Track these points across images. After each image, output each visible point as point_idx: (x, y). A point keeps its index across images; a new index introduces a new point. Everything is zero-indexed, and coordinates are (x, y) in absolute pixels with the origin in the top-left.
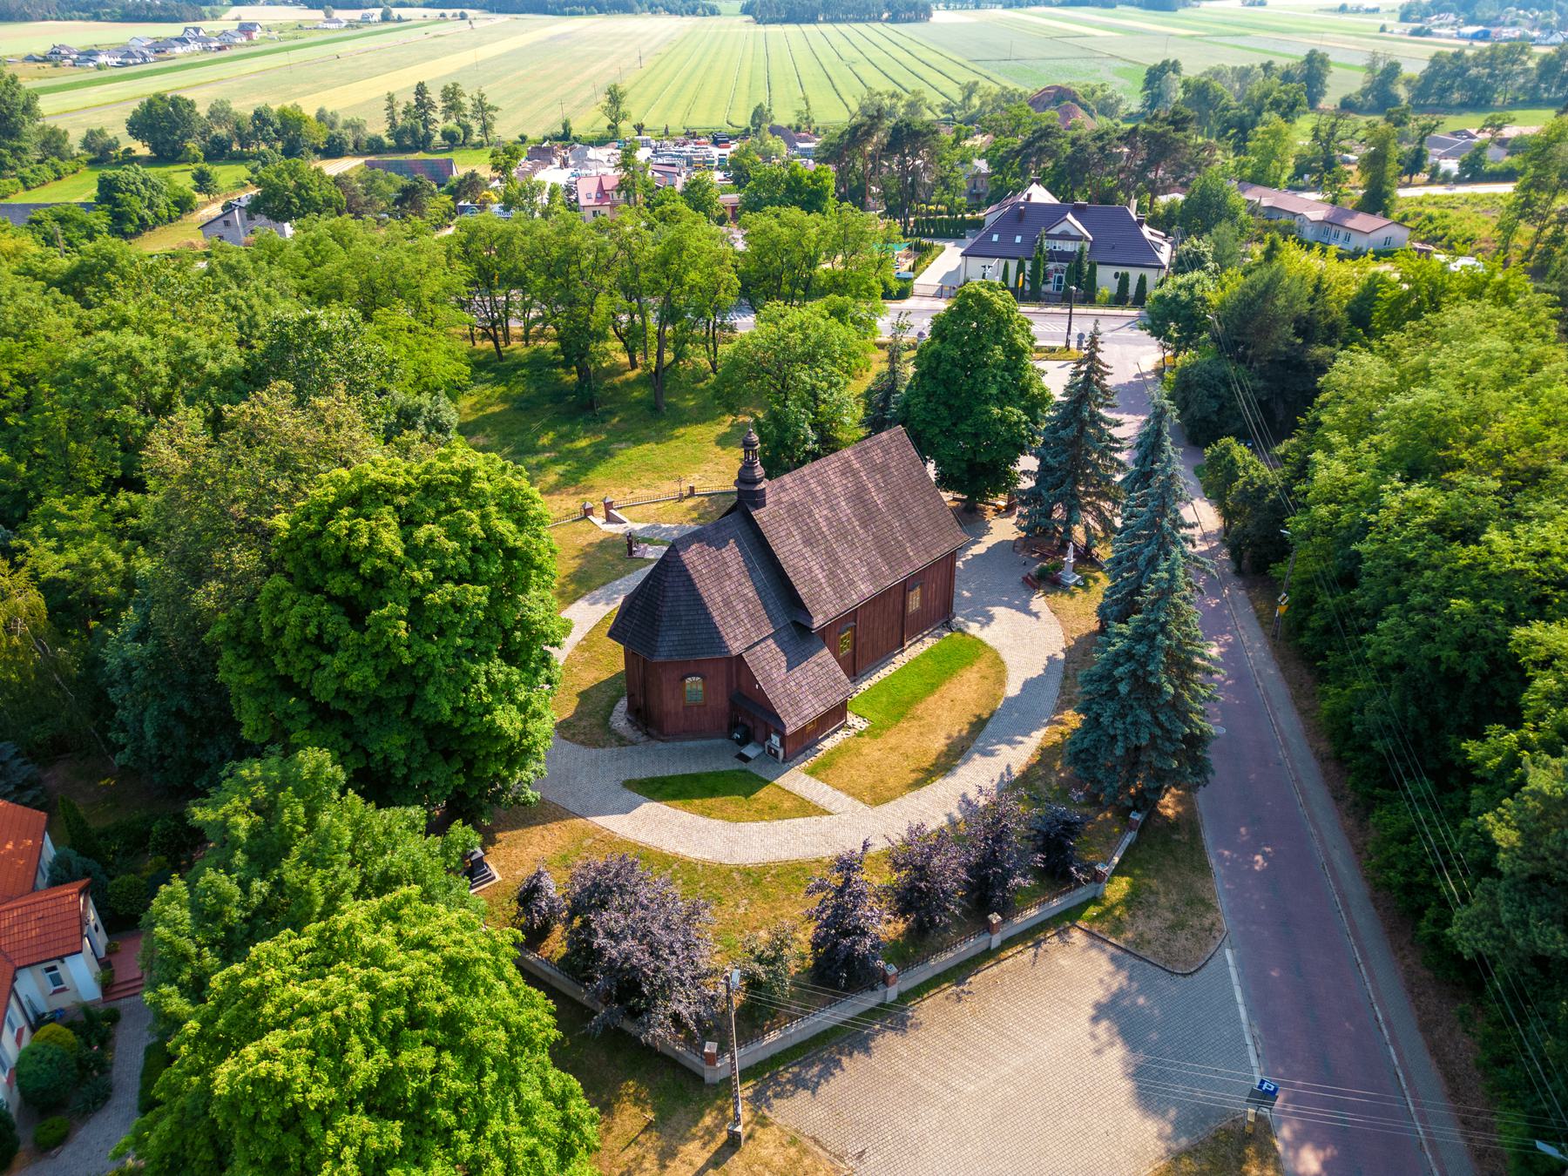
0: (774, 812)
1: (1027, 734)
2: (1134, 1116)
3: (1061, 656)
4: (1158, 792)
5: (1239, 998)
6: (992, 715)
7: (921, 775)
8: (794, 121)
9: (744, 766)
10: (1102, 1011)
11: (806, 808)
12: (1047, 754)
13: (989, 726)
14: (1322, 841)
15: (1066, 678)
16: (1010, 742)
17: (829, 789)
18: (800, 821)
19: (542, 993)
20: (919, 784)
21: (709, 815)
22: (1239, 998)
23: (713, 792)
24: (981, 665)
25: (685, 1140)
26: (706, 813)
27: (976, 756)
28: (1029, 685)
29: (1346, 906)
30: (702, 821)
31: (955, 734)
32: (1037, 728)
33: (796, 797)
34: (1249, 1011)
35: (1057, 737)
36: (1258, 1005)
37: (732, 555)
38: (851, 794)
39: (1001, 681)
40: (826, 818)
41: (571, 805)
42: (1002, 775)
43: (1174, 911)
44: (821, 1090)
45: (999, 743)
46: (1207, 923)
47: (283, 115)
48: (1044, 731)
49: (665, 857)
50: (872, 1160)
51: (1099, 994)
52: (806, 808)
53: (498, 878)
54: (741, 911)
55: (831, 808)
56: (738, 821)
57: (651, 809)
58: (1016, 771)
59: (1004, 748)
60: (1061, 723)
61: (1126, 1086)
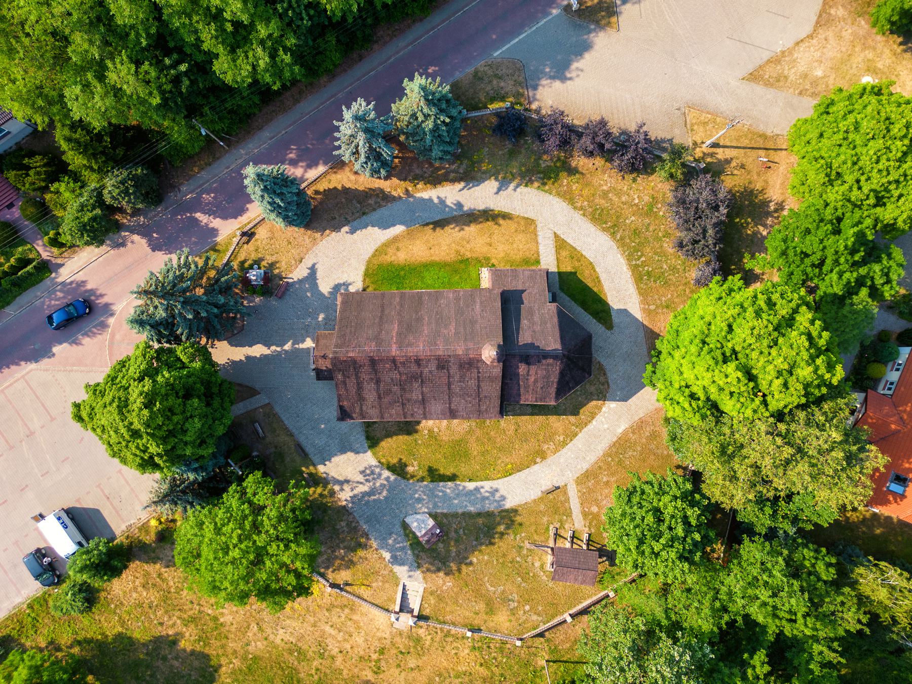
0: (575, 255)
1: (430, 200)
2: (596, 47)
4: (316, 11)
5: (517, 40)
6: (427, 224)
7: (501, 221)
9: (559, 292)
10: (564, 79)
12: (435, 181)
14: (397, 53)
15: (364, 214)
16: (442, 201)
18: (568, 241)
20: (506, 216)
21: (598, 278)
22: (517, 40)
23: (586, 289)
25: (720, 161)
26: (598, 280)
29: (433, 28)
30: (603, 277)
31: (457, 229)
32: (423, 199)
33: (558, 252)
34: (519, 35)
36: (513, 33)
37: (525, 337)
38: (536, 235)
39: (395, 239)
41: (642, 334)
43: (490, 81)
44: (669, 138)
46: (486, 68)
48: (418, 195)
49: (633, 271)
50: (676, 105)
51: (557, 84)
54: (633, 218)
56: (591, 263)
57: (615, 302)
61: (587, 55)
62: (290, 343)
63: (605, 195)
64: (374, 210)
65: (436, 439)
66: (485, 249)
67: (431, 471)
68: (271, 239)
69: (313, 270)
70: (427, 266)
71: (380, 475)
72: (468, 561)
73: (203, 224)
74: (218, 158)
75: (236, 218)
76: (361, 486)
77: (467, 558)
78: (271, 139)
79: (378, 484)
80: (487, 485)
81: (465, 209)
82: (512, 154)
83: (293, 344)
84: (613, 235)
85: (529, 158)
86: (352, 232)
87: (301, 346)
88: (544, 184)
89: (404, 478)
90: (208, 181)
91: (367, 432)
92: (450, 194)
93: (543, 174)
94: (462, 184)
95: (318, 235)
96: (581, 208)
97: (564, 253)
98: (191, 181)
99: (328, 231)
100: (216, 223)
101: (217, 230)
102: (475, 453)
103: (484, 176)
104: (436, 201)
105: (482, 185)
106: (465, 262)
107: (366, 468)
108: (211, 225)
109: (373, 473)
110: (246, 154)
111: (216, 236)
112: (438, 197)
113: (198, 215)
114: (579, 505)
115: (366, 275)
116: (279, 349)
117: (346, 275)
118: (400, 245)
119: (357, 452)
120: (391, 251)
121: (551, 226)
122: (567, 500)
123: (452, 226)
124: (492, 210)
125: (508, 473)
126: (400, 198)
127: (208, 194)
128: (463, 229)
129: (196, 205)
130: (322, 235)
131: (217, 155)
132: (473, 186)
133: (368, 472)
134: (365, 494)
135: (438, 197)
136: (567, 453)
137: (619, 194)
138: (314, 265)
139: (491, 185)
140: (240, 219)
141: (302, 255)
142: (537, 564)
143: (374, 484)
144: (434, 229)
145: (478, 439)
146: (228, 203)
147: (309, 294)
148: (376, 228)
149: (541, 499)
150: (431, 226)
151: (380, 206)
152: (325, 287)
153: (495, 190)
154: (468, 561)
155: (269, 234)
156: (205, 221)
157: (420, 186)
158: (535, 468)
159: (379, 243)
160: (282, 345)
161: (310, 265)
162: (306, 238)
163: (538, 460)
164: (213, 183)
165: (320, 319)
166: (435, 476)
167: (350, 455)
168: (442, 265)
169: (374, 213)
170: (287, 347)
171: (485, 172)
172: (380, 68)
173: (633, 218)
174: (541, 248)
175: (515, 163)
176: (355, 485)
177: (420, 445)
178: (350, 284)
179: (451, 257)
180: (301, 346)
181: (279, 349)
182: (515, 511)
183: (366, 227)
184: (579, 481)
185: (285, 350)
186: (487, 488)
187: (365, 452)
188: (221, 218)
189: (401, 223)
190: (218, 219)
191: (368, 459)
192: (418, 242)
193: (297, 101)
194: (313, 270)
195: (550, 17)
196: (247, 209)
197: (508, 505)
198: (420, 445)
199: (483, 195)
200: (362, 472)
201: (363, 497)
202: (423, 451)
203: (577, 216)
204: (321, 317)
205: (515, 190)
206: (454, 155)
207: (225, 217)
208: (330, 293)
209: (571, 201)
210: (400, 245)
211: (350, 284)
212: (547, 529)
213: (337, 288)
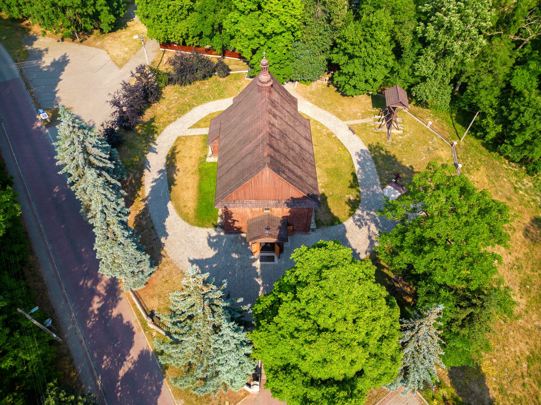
0: (204, 120)
1: (152, 187)
3: (163, 240)
6: (170, 189)
8: (155, 40)
11: (197, 126)
13: (166, 184)
15: (153, 228)
16: (156, 181)
17: (196, 134)
19: (403, 164)
20: (174, 149)
24: (191, 213)
27: (164, 168)
28: (166, 213)
29: (25, 189)
32: (151, 191)
35: (140, 193)
39: (178, 208)
40: (189, 126)
42: (150, 167)
45: (160, 178)
47: (185, 85)
52: (197, 126)
53: (246, 79)
55: (190, 130)
58: (146, 171)
59: (157, 176)
60: (144, 200)
62: (257, 280)
63: (168, 109)
64: (151, 221)
65: (327, 185)
66: (193, 160)
67: (351, 187)
68: (160, 296)
69: (193, 262)
70: (200, 189)
71: (359, 215)
72: (410, 169)
73: (132, 367)
74: (69, 351)
75: (134, 333)
76: (371, 229)
77: (408, 169)
78: (66, 302)
79: (368, 217)
80: (355, 159)
81: (164, 168)
82: (132, 147)
83: (258, 277)
84: (193, 106)
85: (137, 139)
86: (166, 235)
87: (258, 270)
88: (156, 132)
89: (359, 201)
90: (89, 363)
91: (327, 225)
92: (150, 178)
93: (151, 132)
94: (146, 171)
95: (164, 260)
96: (176, 118)
97: (202, 124)
98: (83, 381)
99: (162, 253)
100: (134, 353)
101: (142, 352)
102: (334, 165)
103: (142, 160)
104: (154, 184)
105: (149, 160)
106: (200, 170)
107: (356, 225)
108: (136, 358)
109: (359, 220)
110: (74, 324)
111: (148, 352)
112: (152, 182)
113: (121, 373)
114: (358, 120)
115: (202, 226)
116: (261, 289)
117: (201, 240)
118: (182, 205)
119: (345, 231)
120: (186, 210)
121: (184, 130)
122: (357, 125)
123: (175, 175)
124: (168, 155)
125: (345, 149)
126: (146, 205)
127: (102, 362)
128: (178, 170)
129: (110, 376)
130: (164, 257)
131: (65, 351)
132: (149, 165)
133: (359, 223)
134: (377, 225)
135: (152, 182)
136: (327, 124)
137: (170, 103)
138: (190, 261)
139: (150, 157)
140: (135, 329)
141: (179, 272)
142: (401, 137)
143: (367, 220)
144: (175, 185)
145: (325, 163)
146: (117, 341)
147: (214, 265)
148: (167, 219)
149: (358, 135)
150: (172, 187)
151: (150, 217)
152: (210, 253)
153: (155, 154)
154: (410, 169)
155: (156, 299)
156: (130, 365)
157: (140, 193)
158: (339, 137)
159: (179, 218)
160: (259, 286)
161: (190, 264)
162: (165, 268)
163: (334, 136)
164: (92, 356)
165: (237, 257)
166: (354, 184)
167: (348, 235)
168: (201, 179)
169: (154, 221)
170: (260, 282)
171: (140, 160)
172: (40, 221)
173: (186, 99)
174: (197, 134)
175: (139, 145)
176: (371, 232)
177: (333, 193)
178: (209, 235)
179: (197, 177)
180: (258, 270)
181: (261, 289)
182: (369, 146)
183: (164, 227)
184: (344, 120)
185: (263, 283)
186: (357, 157)
187: (344, 226)
188: (130, 348)
189: (166, 203)
190: (131, 351)
191: (349, 223)
192: (182, 195)
193: (41, 280)
194: (193, 262)
195: (49, 134)
196: (128, 322)
197: (365, 148)
198: (333, 193)
199: (156, 161)
200: (360, 227)
201: (380, 228)
202: (337, 191)
203: (179, 120)
204: (235, 256)
205: (157, 145)
206: (147, 85)
207: (130, 344)
208: (214, 250)
209: (170, 122)
210: (182, 205)
211: (209, 235)
212: (377, 133)
213: (211, 244)
